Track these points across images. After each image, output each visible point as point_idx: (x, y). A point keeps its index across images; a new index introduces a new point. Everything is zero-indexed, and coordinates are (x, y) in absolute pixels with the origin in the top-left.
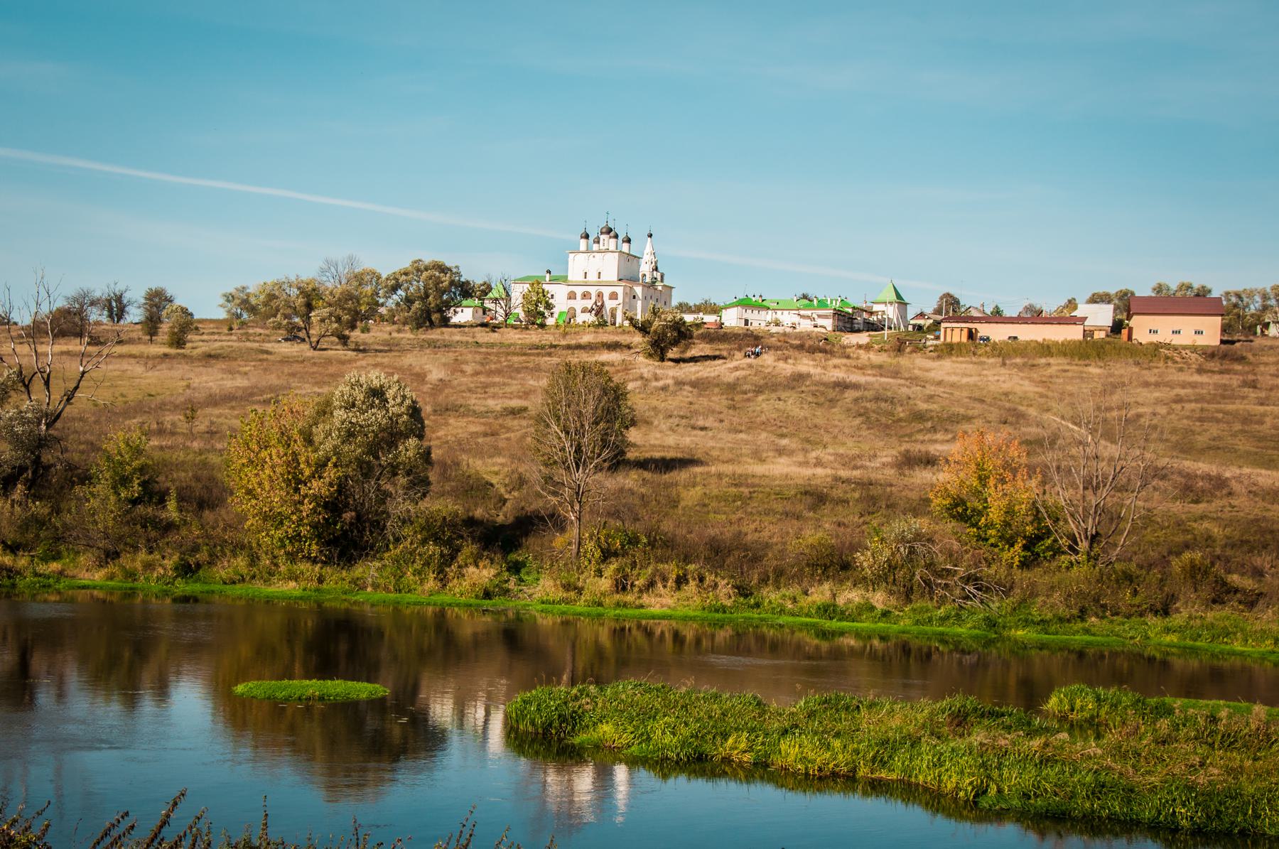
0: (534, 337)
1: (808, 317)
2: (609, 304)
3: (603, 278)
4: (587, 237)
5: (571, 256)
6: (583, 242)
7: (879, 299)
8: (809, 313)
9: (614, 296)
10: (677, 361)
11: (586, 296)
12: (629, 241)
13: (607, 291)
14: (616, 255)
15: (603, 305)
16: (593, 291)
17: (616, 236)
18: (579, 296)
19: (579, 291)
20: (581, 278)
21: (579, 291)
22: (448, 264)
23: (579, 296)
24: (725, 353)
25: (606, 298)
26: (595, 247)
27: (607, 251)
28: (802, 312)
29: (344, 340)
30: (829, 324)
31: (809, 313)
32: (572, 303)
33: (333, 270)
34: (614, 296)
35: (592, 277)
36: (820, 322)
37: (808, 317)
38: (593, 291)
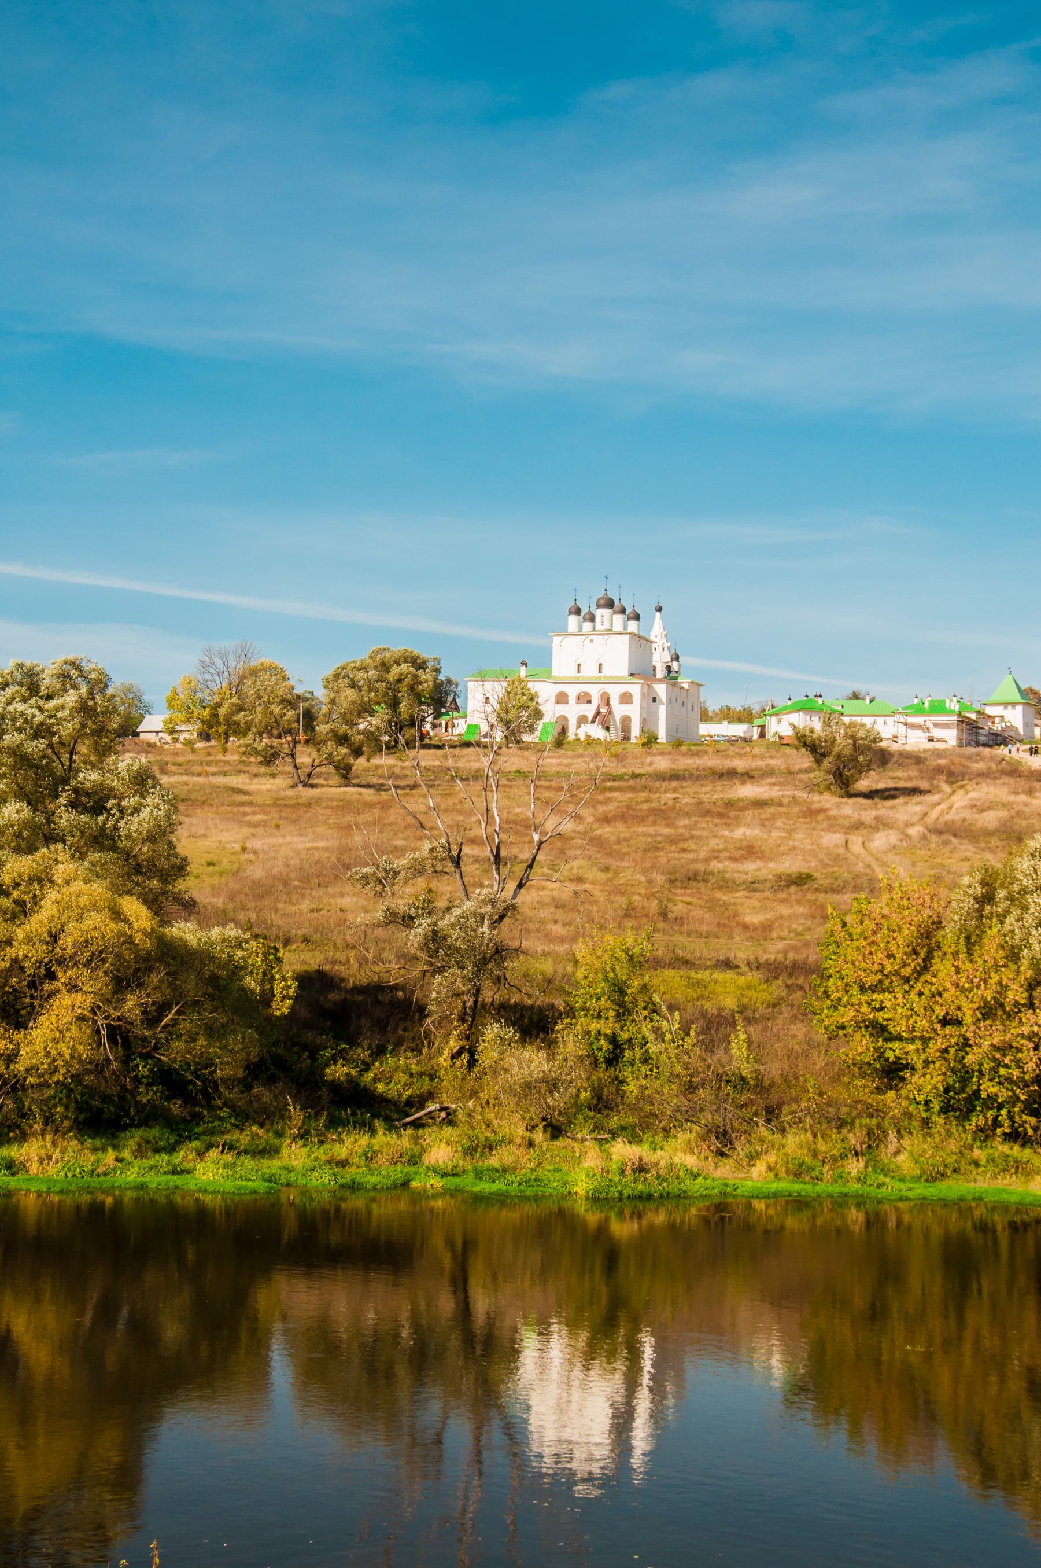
0: (513, 760)
1: (919, 727)
2: (619, 711)
3: (607, 672)
4: (578, 611)
5: (556, 640)
6: (573, 621)
7: (995, 697)
8: (920, 720)
9: (626, 699)
10: (870, 795)
11: (585, 699)
12: (637, 617)
13: (615, 692)
14: (627, 637)
15: (610, 712)
16: (595, 691)
17: (623, 611)
18: (572, 699)
19: (572, 691)
20: (572, 672)
21: (572, 691)
22: (425, 655)
23: (572, 699)
24: (923, 785)
25: (614, 702)
26: (587, 627)
27: (609, 632)
28: (910, 720)
29: (345, 772)
30: (951, 737)
31: (920, 720)
32: (561, 710)
33: (219, 663)
34: (626, 699)
35: (590, 671)
36: (937, 733)
37: (919, 727)
38: (595, 691)
